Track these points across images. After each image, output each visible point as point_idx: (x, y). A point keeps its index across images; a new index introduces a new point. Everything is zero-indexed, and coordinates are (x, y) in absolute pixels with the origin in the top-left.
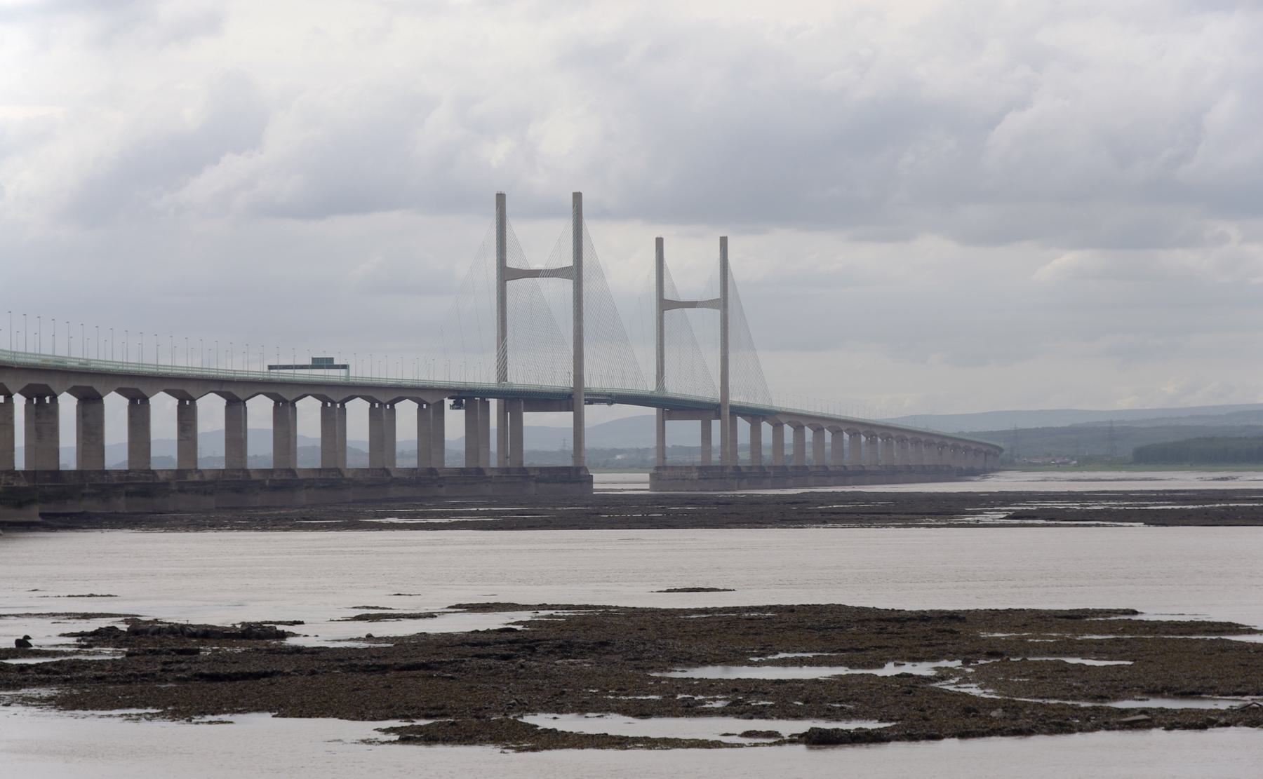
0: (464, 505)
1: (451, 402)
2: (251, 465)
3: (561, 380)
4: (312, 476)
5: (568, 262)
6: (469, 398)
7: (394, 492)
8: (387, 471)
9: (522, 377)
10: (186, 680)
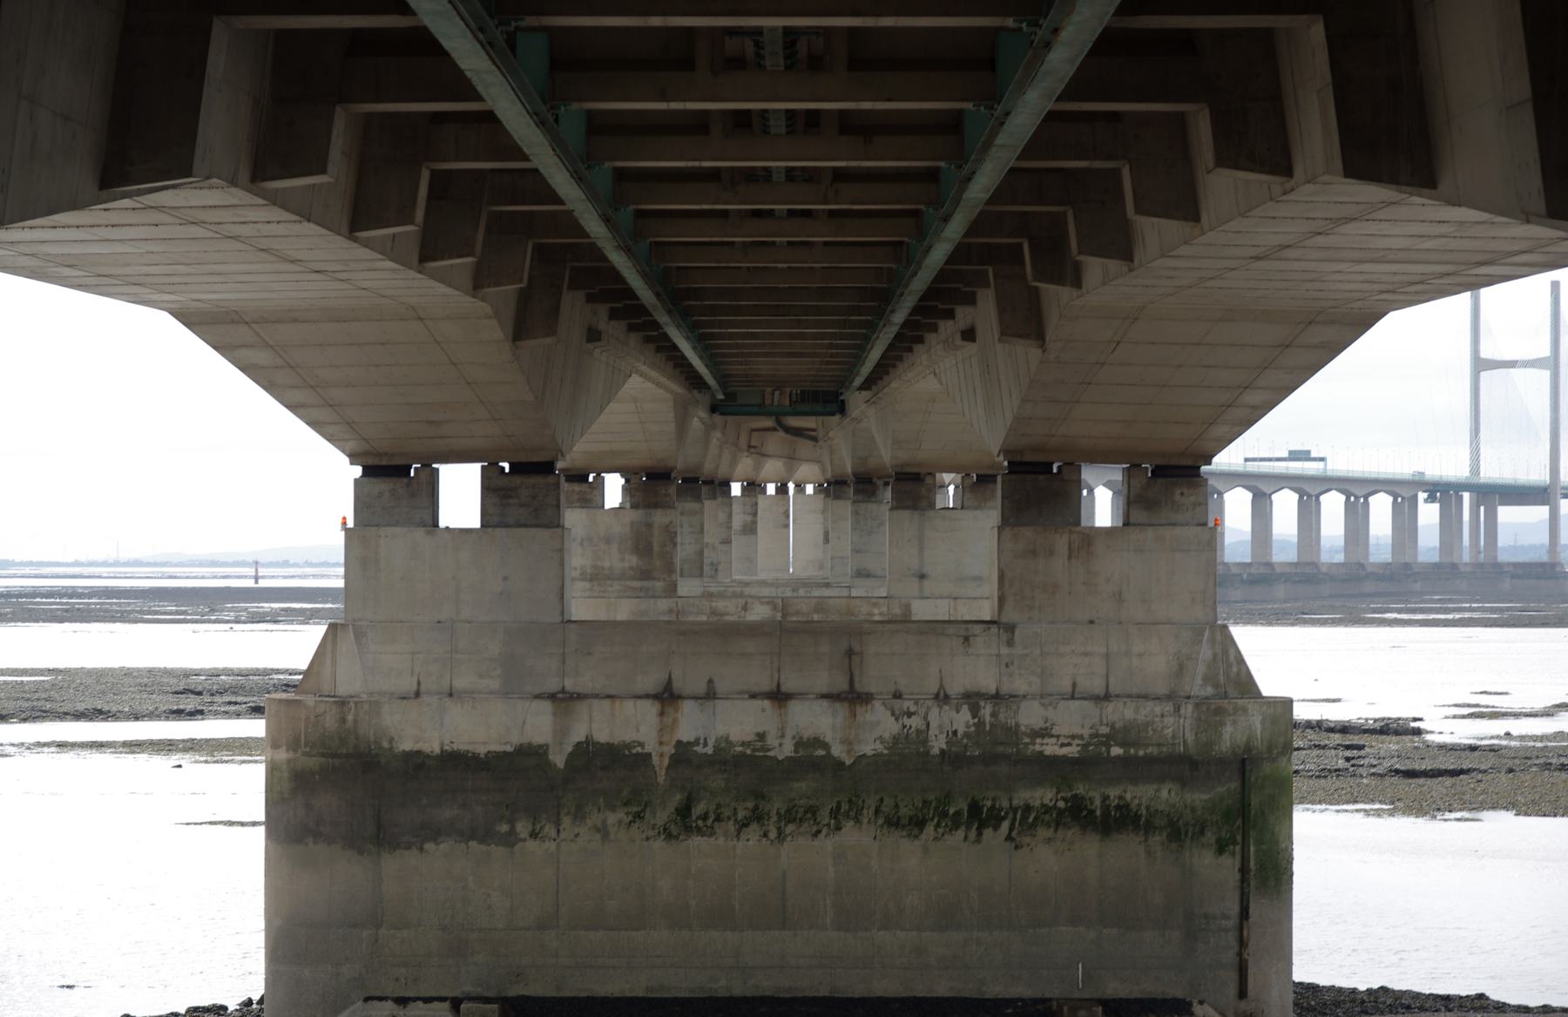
0: (1450, 601)
1: (1425, 495)
2: (1325, 558)
3: (1537, 474)
4: (1288, 570)
5: (1546, 352)
6: (1443, 492)
7: (1369, 587)
8: (1361, 566)
9: (1495, 470)
10: (1381, 776)
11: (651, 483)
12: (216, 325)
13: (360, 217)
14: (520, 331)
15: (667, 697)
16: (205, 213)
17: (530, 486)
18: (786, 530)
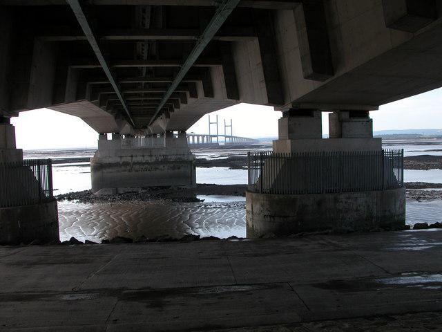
9: (212, 134)
11: (128, 136)
12: (86, 119)
13: (100, 105)
14: (116, 118)
15: (132, 156)
16: (85, 104)
17: (117, 135)
18: (141, 140)
